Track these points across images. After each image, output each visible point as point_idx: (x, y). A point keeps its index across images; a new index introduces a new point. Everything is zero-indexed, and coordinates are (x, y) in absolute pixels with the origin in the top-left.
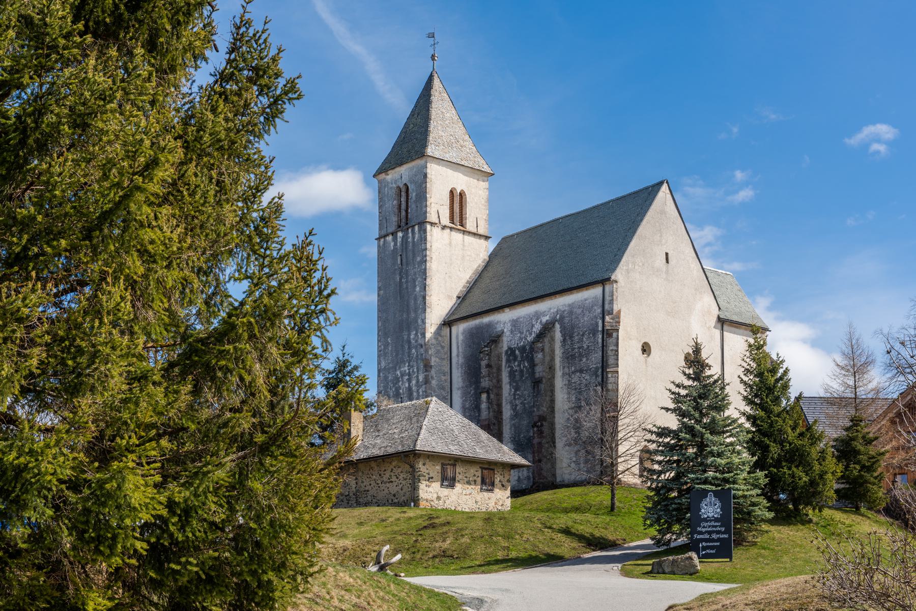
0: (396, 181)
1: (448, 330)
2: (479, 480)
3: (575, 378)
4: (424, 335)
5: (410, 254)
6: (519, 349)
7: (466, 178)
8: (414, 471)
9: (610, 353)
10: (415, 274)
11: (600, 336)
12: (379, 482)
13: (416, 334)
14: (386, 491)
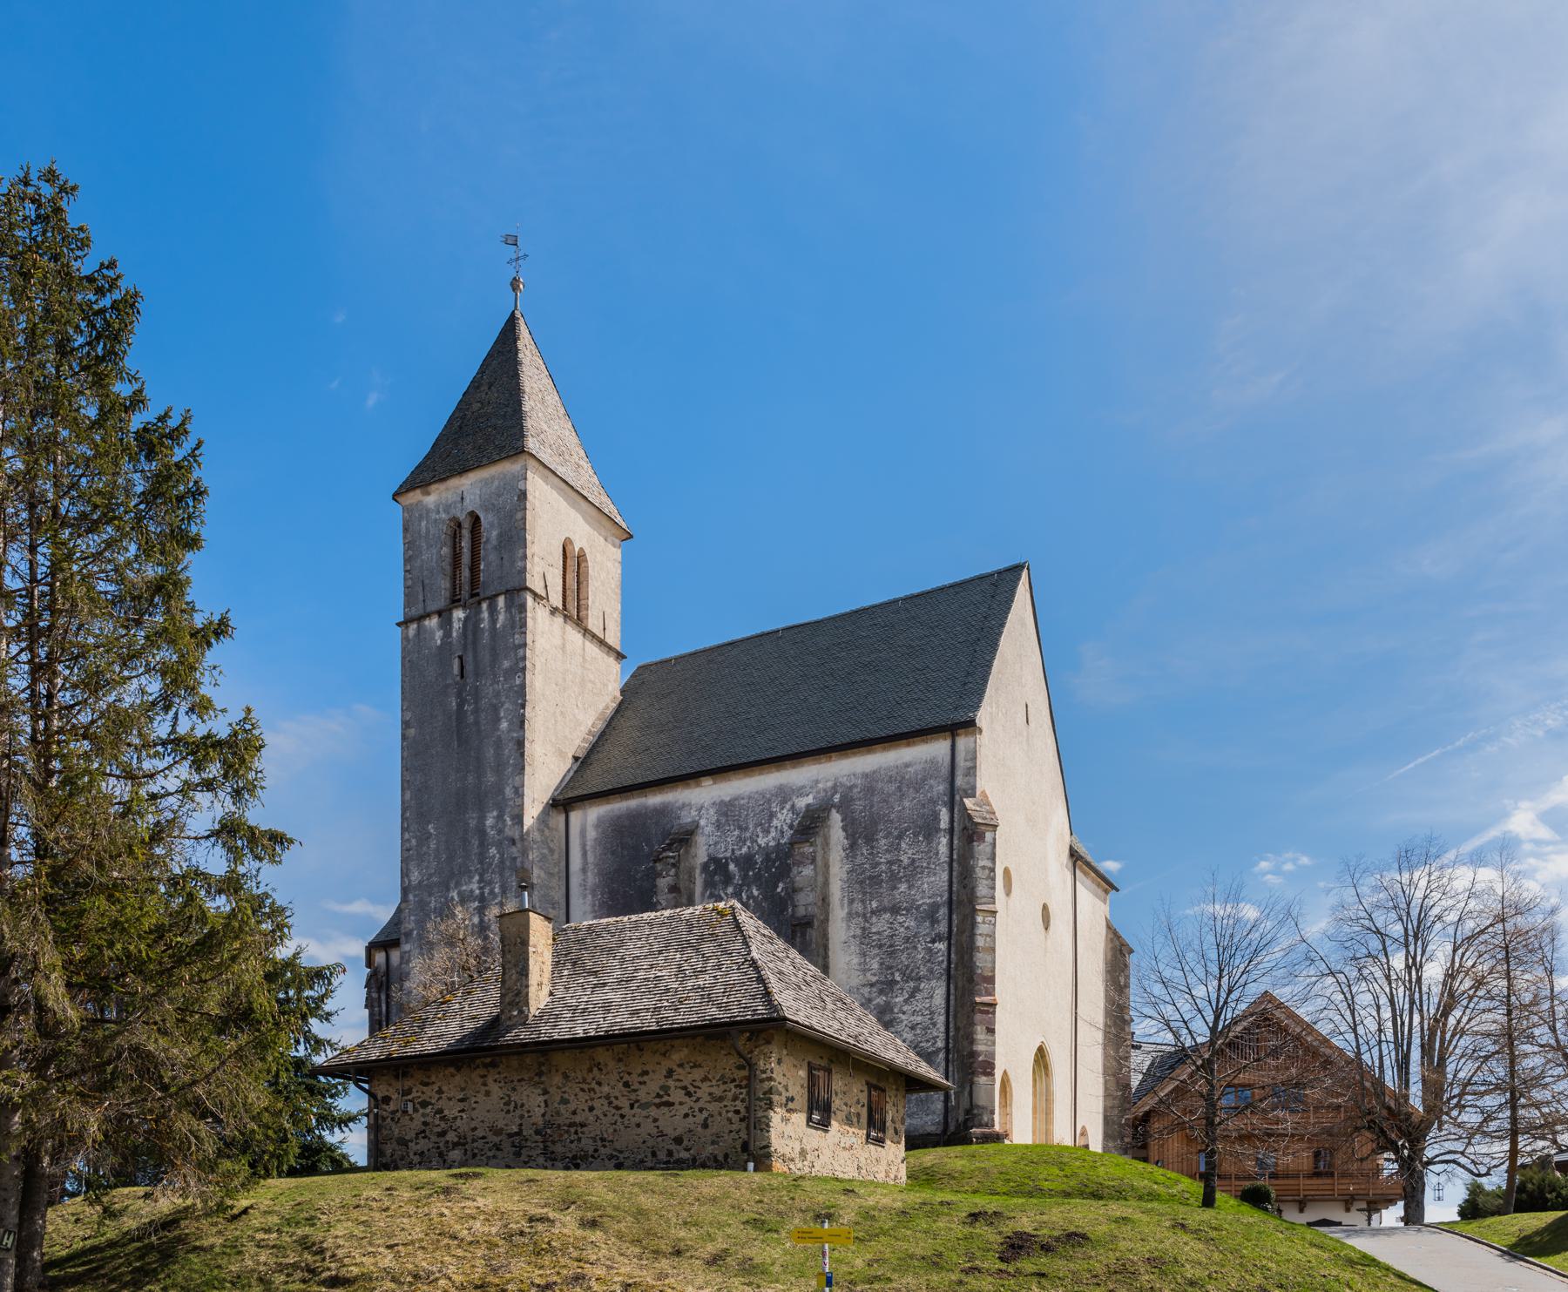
0: (447, 509)
1: (562, 818)
2: (864, 1120)
3: (880, 924)
4: (519, 819)
5: (486, 657)
6: (736, 861)
7: (587, 527)
8: (750, 1079)
9: (979, 873)
10: (497, 695)
11: (944, 841)
12: (624, 1103)
13: (500, 817)
14: (649, 1127)
